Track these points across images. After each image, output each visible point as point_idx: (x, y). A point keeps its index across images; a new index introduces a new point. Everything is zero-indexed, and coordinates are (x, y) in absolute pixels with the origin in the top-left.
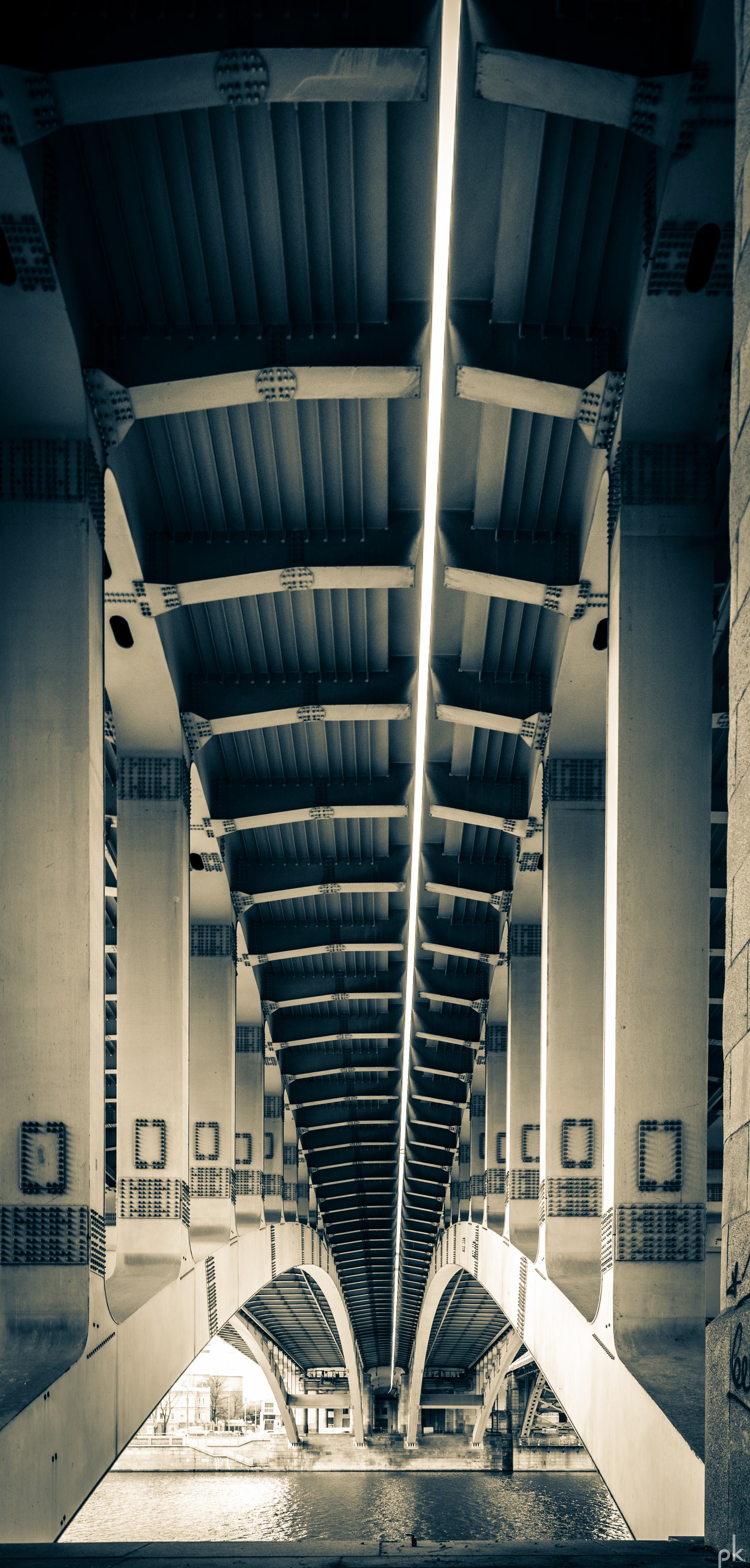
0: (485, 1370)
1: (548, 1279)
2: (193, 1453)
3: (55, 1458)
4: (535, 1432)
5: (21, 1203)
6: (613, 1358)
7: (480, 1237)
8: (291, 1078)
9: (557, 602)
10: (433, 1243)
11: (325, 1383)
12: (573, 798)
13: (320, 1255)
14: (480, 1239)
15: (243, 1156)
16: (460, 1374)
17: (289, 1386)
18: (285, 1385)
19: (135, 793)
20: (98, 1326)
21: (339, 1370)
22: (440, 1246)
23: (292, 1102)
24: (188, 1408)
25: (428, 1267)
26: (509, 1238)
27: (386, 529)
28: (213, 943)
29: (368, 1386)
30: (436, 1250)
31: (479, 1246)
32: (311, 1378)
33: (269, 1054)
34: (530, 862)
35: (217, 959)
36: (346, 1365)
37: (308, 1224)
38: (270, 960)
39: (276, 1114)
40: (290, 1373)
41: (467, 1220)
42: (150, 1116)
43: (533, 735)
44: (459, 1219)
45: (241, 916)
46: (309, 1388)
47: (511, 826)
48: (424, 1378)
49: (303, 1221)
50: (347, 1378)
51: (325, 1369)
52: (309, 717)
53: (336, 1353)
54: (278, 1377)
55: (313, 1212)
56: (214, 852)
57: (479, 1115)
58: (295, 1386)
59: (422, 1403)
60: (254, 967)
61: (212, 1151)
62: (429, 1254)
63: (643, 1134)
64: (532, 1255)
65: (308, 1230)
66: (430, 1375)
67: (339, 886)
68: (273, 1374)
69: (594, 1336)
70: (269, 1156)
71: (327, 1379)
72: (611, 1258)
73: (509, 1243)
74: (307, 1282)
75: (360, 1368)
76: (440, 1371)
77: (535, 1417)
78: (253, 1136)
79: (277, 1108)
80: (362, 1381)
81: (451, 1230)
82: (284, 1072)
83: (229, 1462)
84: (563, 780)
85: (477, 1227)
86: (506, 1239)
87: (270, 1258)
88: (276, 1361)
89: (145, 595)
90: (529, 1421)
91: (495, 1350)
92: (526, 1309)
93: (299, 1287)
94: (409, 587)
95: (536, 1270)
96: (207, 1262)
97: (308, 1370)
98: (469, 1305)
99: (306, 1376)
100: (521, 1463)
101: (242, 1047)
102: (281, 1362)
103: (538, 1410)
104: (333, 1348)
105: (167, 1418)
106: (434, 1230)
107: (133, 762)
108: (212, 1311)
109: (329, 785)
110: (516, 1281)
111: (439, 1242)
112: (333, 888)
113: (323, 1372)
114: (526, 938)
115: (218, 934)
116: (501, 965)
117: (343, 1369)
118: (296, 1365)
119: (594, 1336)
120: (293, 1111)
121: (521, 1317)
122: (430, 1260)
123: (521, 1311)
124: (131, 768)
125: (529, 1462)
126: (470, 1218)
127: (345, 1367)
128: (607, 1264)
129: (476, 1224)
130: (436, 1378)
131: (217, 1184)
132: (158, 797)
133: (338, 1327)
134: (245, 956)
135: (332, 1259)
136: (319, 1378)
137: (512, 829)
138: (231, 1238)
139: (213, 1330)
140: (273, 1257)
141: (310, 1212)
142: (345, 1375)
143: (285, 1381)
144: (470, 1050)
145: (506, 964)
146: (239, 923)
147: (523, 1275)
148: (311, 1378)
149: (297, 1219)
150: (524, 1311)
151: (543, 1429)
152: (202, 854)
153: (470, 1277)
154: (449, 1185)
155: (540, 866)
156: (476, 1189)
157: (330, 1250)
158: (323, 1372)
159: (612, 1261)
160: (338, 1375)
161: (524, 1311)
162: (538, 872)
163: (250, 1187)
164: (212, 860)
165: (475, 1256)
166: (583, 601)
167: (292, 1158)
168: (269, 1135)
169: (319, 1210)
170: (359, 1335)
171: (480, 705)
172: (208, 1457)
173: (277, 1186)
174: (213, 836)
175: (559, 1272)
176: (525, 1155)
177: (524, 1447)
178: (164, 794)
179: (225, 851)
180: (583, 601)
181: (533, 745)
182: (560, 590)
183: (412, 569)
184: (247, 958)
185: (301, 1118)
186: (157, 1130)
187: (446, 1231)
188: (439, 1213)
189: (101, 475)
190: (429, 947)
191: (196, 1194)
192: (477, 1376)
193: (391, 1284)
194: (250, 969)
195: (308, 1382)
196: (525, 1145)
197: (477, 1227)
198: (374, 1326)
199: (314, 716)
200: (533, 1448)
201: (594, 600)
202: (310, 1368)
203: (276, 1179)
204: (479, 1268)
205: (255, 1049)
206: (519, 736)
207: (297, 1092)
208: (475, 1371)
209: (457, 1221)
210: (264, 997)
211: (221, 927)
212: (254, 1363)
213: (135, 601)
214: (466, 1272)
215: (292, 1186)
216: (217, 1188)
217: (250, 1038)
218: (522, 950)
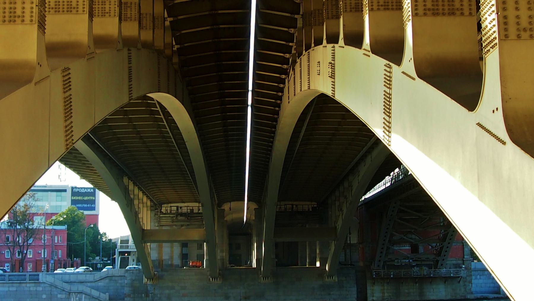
0: (337, 203)
1: (417, 79)
2: (50, 289)
4: (388, 263)
10: (285, 75)
11: (180, 218)
17: (145, 222)
18: (141, 220)
22: (293, 76)
24: (51, 290)
30: (288, 81)
32: (165, 214)
40: (145, 209)
44: (313, 45)
62: (282, 86)
69: (479, 124)
71: (182, 214)
73: (370, 54)
76: (293, 205)
77: (388, 248)
81: (304, 58)
88: (132, 196)
91: (346, 184)
99: (161, 212)
100: (375, 295)
102: (136, 197)
103: (390, 241)
105: (24, 255)
106: (286, 61)
108: (69, 122)
111: (291, 72)
113: (177, 207)
118: (151, 201)
119: (479, 124)
122: (283, 92)
125: (383, 293)
126: (325, 42)
128: (491, 46)
129: (332, 45)
136: (174, 214)
139: (68, 142)
147: (388, 81)
148: (165, 214)
150: (390, 117)
154: (300, 16)
156: (330, 13)
160: (192, 210)
161: (390, 117)
172: (64, 292)
187: (298, 60)
188: (291, 44)
191: (52, 11)
197: (334, 47)
203: (133, 6)
209: (310, 48)
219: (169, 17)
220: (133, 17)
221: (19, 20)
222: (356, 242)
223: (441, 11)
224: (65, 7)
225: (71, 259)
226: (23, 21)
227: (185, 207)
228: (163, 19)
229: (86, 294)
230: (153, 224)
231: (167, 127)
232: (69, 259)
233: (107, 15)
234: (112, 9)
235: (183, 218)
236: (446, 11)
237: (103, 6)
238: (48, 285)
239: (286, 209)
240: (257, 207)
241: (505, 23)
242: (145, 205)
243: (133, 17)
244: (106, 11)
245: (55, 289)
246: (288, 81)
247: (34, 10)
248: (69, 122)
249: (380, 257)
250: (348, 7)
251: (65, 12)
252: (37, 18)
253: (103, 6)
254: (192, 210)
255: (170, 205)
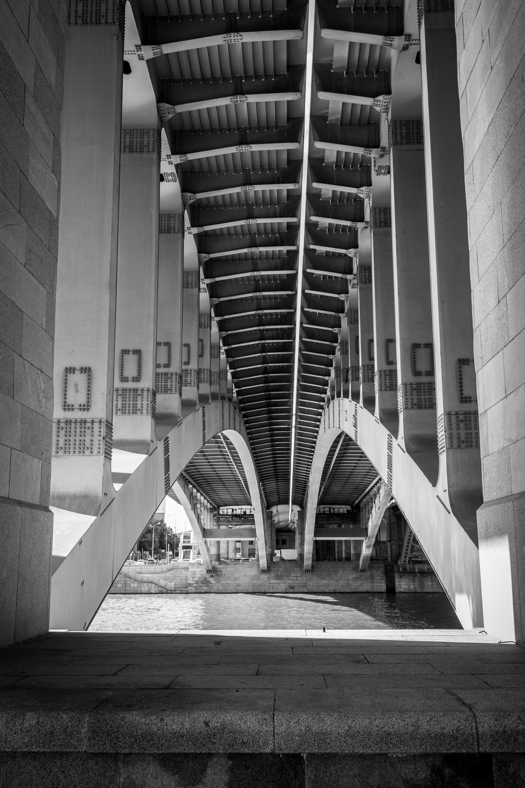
2: (124, 579)
3: (83, 583)
5: (62, 418)
6: (449, 513)
7: (358, 412)
8: (216, 301)
9: (391, 44)
12: (408, 143)
13: (235, 421)
14: (358, 414)
15: (185, 360)
16: (347, 511)
19: (127, 150)
20: (107, 494)
21: (246, 508)
22: (327, 413)
23: (216, 316)
25: (318, 426)
26: (379, 418)
27: (286, 9)
28: (169, 225)
29: (270, 521)
30: (325, 415)
31: (358, 419)
32: (222, 515)
33: (203, 286)
34: (383, 171)
35: (171, 235)
36: (253, 504)
37: (227, 400)
38: (205, 230)
39: (206, 326)
40: (206, 511)
41: (348, 397)
42: (131, 347)
43: (380, 106)
45: (187, 206)
46: (222, 523)
47: (369, 152)
48: (317, 514)
49: (223, 398)
50: (253, 515)
51: (235, 507)
52: (237, 101)
53: (243, 493)
54: (197, 514)
55: (230, 389)
56: (172, 172)
57: (354, 323)
58: (208, 522)
59: (315, 536)
60: (194, 235)
61: (166, 362)
63: (460, 367)
64: (394, 432)
65: (227, 405)
66: (322, 510)
67: (254, 187)
68: (193, 512)
69: (438, 497)
70: (201, 355)
71: (236, 516)
72: (444, 447)
73: (379, 421)
74: (222, 440)
75: (264, 507)
76: (330, 508)
78: (191, 345)
79: (206, 322)
80: (265, 518)
82: (211, 296)
83: (155, 587)
84: (401, 133)
85: (356, 405)
86: (377, 419)
87: (202, 430)
89: (141, 51)
90: (407, 550)
92: (393, 471)
93: (216, 443)
94: (300, 38)
95: (398, 445)
96: (165, 441)
97: (221, 508)
98: (350, 453)
99: (219, 514)
101: (186, 285)
104: (242, 490)
106: (322, 408)
107: (126, 132)
108: (167, 475)
109: (248, 131)
110: (385, 451)
112: (250, 188)
113: (233, 510)
114: (382, 216)
115: (172, 220)
116: (366, 228)
117: (249, 507)
119: (438, 497)
120: (217, 321)
121: (390, 477)
123: (390, 473)
124: (125, 136)
127: (251, 505)
130: (327, 514)
131: (169, 384)
132: (141, 151)
133: (246, 473)
134: (189, 229)
135: (242, 422)
137: (370, 153)
138: (179, 421)
140: (204, 429)
141: (227, 389)
142: (251, 512)
143: (202, 517)
144: (347, 280)
145: (369, 228)
146: (186, 210)
149: (219, 398)
150: (391, 472)
151: (420, 557)
152: (164, 173)
153: (350, 439)
154: (333, 368)
155: (389, 173)
157: (242, 416)
158: (233, 510)
159: (445, 449)
160: (245, 512)
161: (391, 472)
162: (388, 175)
163: (189, 381)
164: (171, 177)
165: (355, 426)
166: (407, 43)
167: (216, 354)
168: (201, 341)
169: (234, 387)
170: (262, 478)
171: (346, 90)
172: (136, 582)
173: (206, 376)
174: (172, 164)
175: (413, 448)
176: (388, 360)
177: (404, 573)
178: (146, 150)
179: (178, 170)
180: (407, 43)
181: (381, 111)
182: (392, 38)
183: (301, 30)
184: (190, 230)
185: (222, 326)
186: (136, 356)
189: (124, 5)
190: (314, 219)
192: (361, 512)
193: (289, 440)
194: (192, 236)
195: (218, 518)
196: (388, 349)
198: (275, 470)
199: (240, 100)
200: (412, 573)
201: (414, 42)
202: (222, 506)
204: (358, 435)
205: (194, 286)
206: (371, 107)
207: (219, 309)
208: (359, 507)
210: (200, 251)
211: (175, 215)
212: (176, 502)
213: (135, 54)
214: (347, 435)
215: (216, 374)
216: (169, 387)
217: (190, 279)
218: (380, 224)
219: (216, 316)
220: (206, 380)
221: (139, 412)
222: (385, 540)
223: (423, 406)
224: (163, 389)
225: (141, 552)
226: (142, 413)
227: (239, 509)
228: (218, 348)
229: (155, 584)
230: (212, 523)
231: (222, 438)
232: (139, 552)
233: (189, 385)
234: (193, 381)
235: (237, 519)
236: (427, 406)
237: (186, 378)
238: (123, 576)
239: (324, 512)
240: (300, 509)
241: (452, 438)
242: (206, 508)
243: (206, 380)
244: (188, 382)
245: (128, 579)
246: (325, 415)
247: (149, 406)
248: (167, 475)
249: (406, 553)
250: (366, 379)
251: (163, 393)
252: (151, 411)
253: (186, 378)
254: (245, 512)
255: (226, 507)
